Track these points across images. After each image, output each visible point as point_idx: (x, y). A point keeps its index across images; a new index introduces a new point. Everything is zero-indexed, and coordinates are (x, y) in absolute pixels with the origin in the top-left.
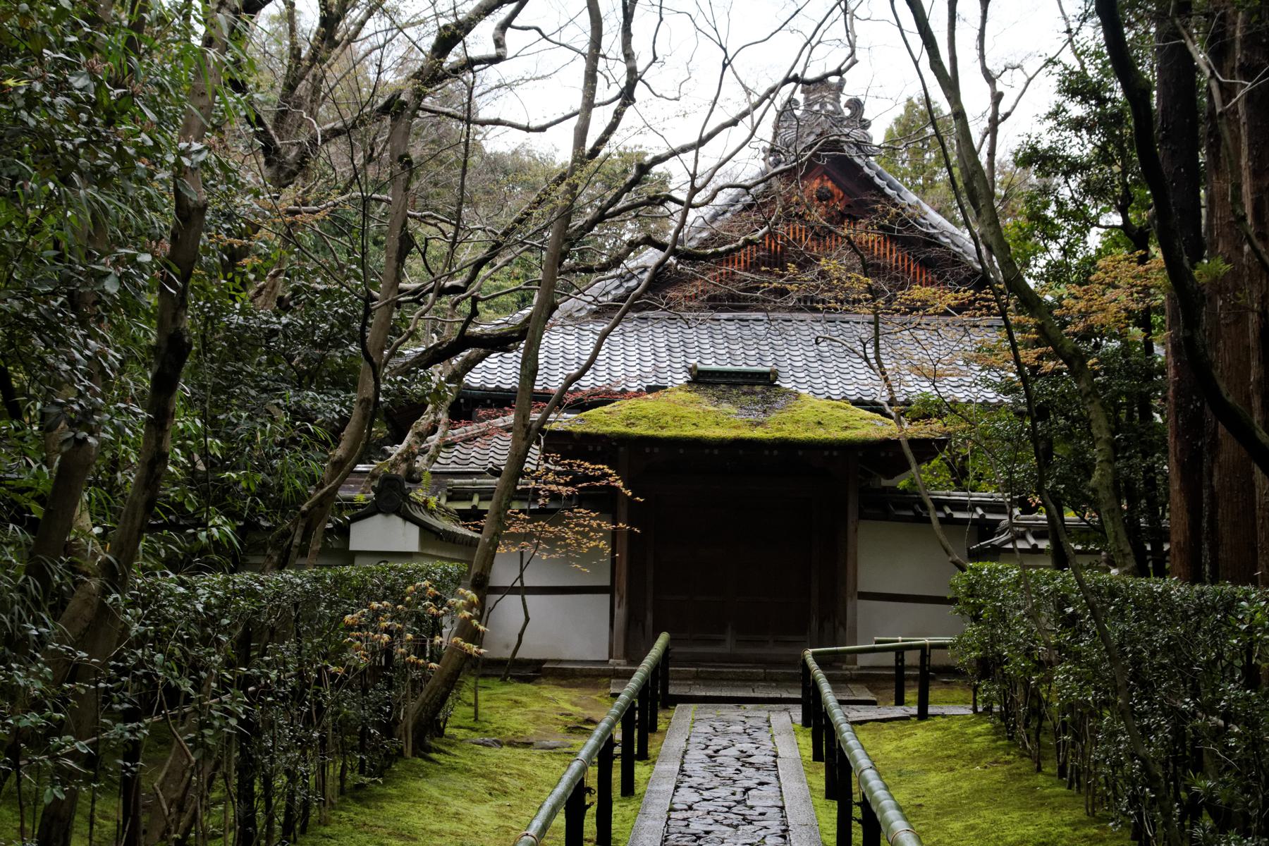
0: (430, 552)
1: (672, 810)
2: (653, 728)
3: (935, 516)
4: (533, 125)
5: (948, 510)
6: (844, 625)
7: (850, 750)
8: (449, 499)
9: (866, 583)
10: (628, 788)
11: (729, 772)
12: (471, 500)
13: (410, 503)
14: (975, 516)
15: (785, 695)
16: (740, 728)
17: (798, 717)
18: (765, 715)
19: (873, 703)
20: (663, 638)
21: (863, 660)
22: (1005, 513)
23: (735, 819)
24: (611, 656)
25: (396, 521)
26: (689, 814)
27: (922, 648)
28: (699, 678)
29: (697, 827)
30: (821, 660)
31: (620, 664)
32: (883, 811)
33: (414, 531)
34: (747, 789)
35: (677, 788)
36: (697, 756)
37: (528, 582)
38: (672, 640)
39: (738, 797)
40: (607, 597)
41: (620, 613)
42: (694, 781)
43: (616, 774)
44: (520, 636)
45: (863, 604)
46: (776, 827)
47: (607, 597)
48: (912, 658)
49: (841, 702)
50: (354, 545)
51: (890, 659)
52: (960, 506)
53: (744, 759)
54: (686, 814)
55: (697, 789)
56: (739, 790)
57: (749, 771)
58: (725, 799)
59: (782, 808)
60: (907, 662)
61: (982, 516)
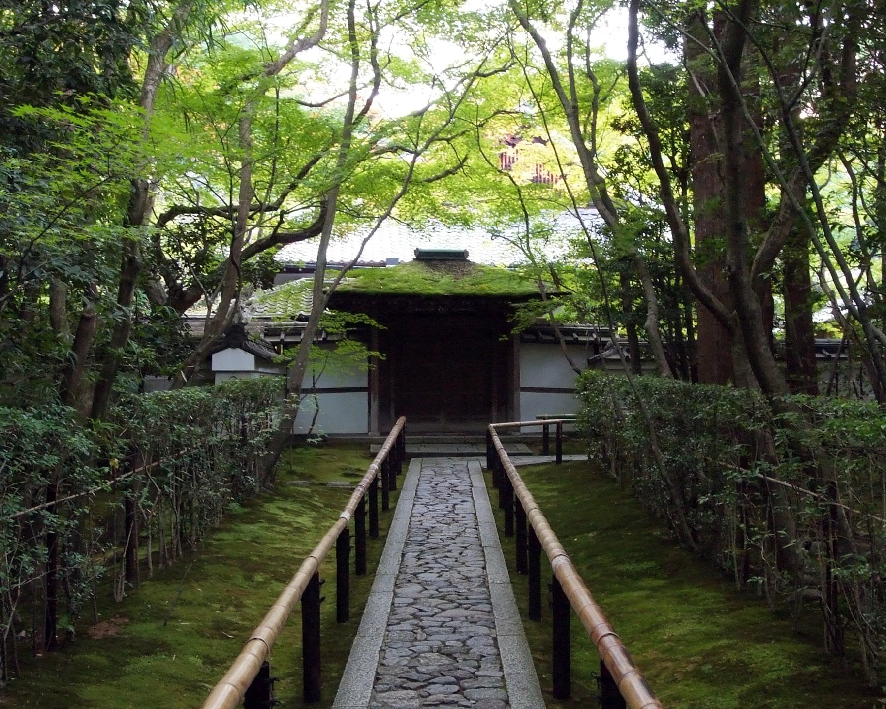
0: (261, 370)
1: (388, 625)
2: (393, 487)
3: (563, 339)
4: (313, 103)
5: (575, 336)
6: (512, 408)
7: (621, 676)
8: (266, 335)
9: (523, 384)
10: (385, 507)
11: (445, 495)
12: (279, 335)
13: (248, 340)
14: (591, 339)
15: (477, 451)
16: (450, 471)
17: (484, 464)
18: (465, 463)
19: (530, 455)
20: (402, 420)
21: (524, 430)
22: (609, 336)
23: (448, 520)
24: (369, 431)
25: (239, 352)
26: (422, 518)
27: (557, 423)
28: (423, 442)
29: (427, 524)
30: (500, 432)
31: (377, 436)
32: (513, 478)
33: (251, 358)
34: (455, 505)
35: (414, 505)
36: (425, 486)
37: (317, 386)
38: (408, 421)
39: (449, 509)
40: (366, 393)
41: (375, 405)
42: (424, 501)
43: (380, 499)
44: (314, 420)
45: (522, 394)
46: (471, 524)
47: (366, 393)
48: (553, 429)
49: (509, 455)
50: (215, 367)
51: (540, 429)
52: (582, 333)
53: (453, 488)
54: (420, 519)
55: (426, 505)
56: (450, 506)
57: (456, 495)
58: (442, 510)
59: (475, 514)
60: (550, 431)
61: (596, 339)
